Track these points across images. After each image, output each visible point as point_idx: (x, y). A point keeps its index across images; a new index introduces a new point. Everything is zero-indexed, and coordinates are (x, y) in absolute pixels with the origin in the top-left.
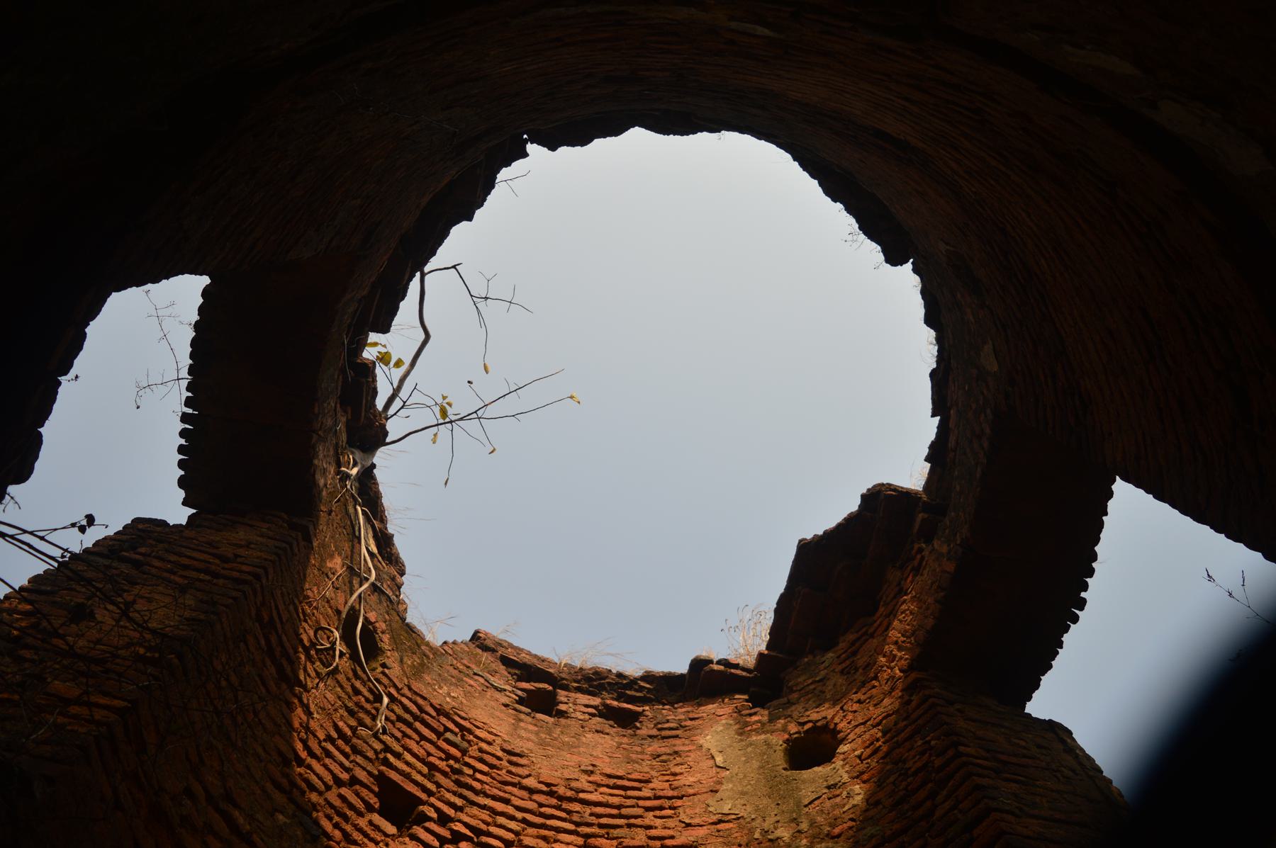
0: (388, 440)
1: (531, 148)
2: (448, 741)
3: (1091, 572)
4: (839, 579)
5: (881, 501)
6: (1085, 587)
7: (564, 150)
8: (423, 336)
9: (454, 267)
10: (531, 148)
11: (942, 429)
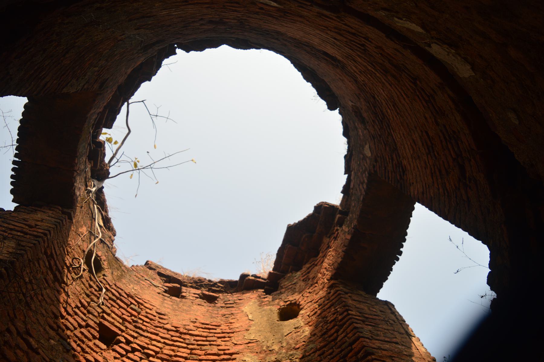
0: (110, 176)
1: (178, 51)
2: (132, 309)
3: (405, 240)
4: (302, 243)
5: (322, 209)
6: (402, 246)
7: (192, 53)
8: (127, 131)
9: (143, 101)
10: (178, 51)
11: (349, 180)
